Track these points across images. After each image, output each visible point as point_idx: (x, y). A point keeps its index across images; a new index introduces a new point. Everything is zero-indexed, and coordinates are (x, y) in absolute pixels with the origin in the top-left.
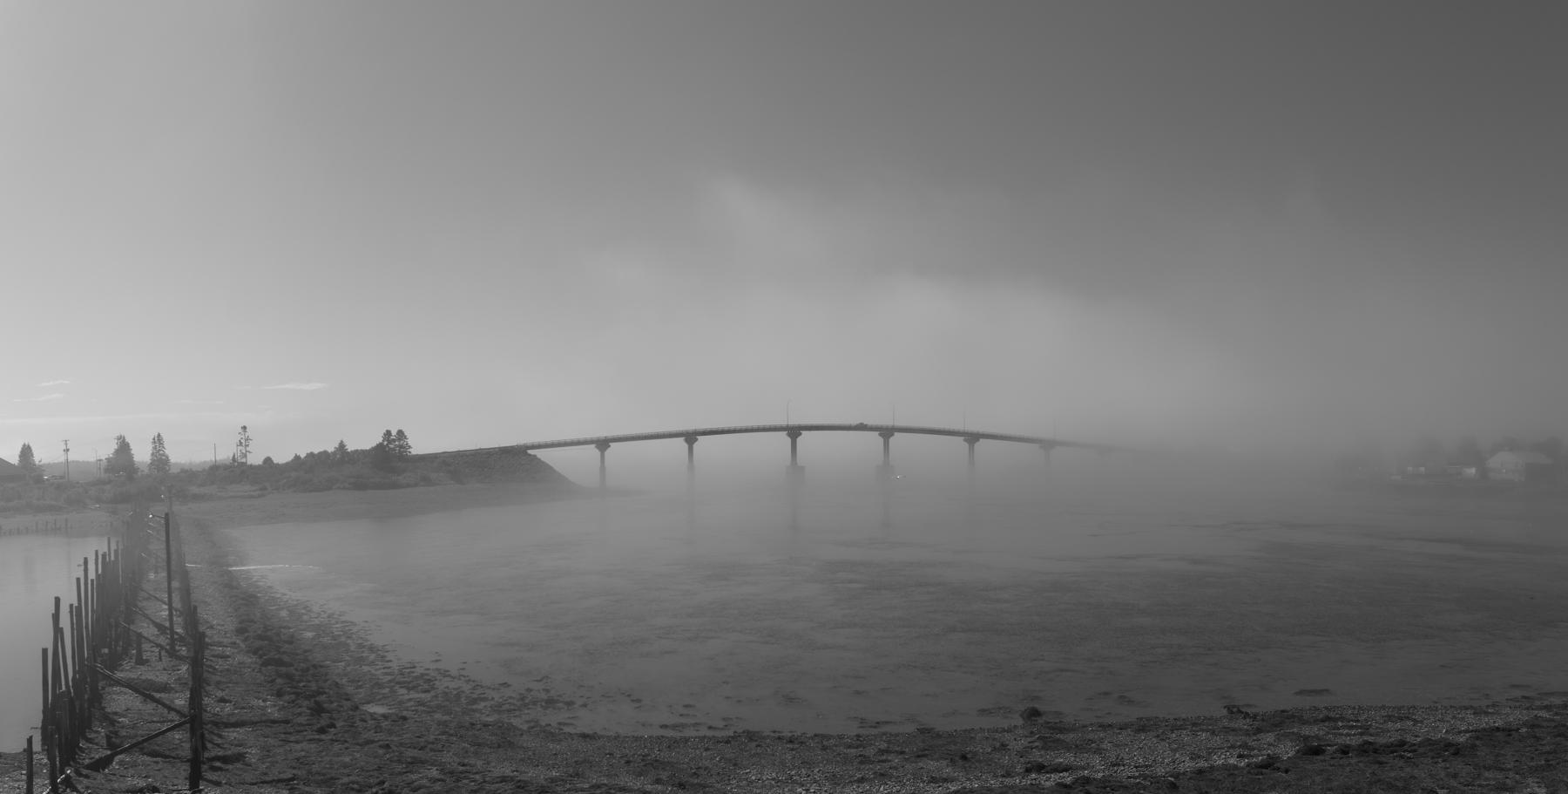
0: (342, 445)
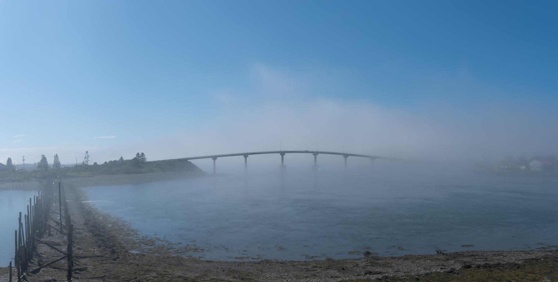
0: (122, 158)
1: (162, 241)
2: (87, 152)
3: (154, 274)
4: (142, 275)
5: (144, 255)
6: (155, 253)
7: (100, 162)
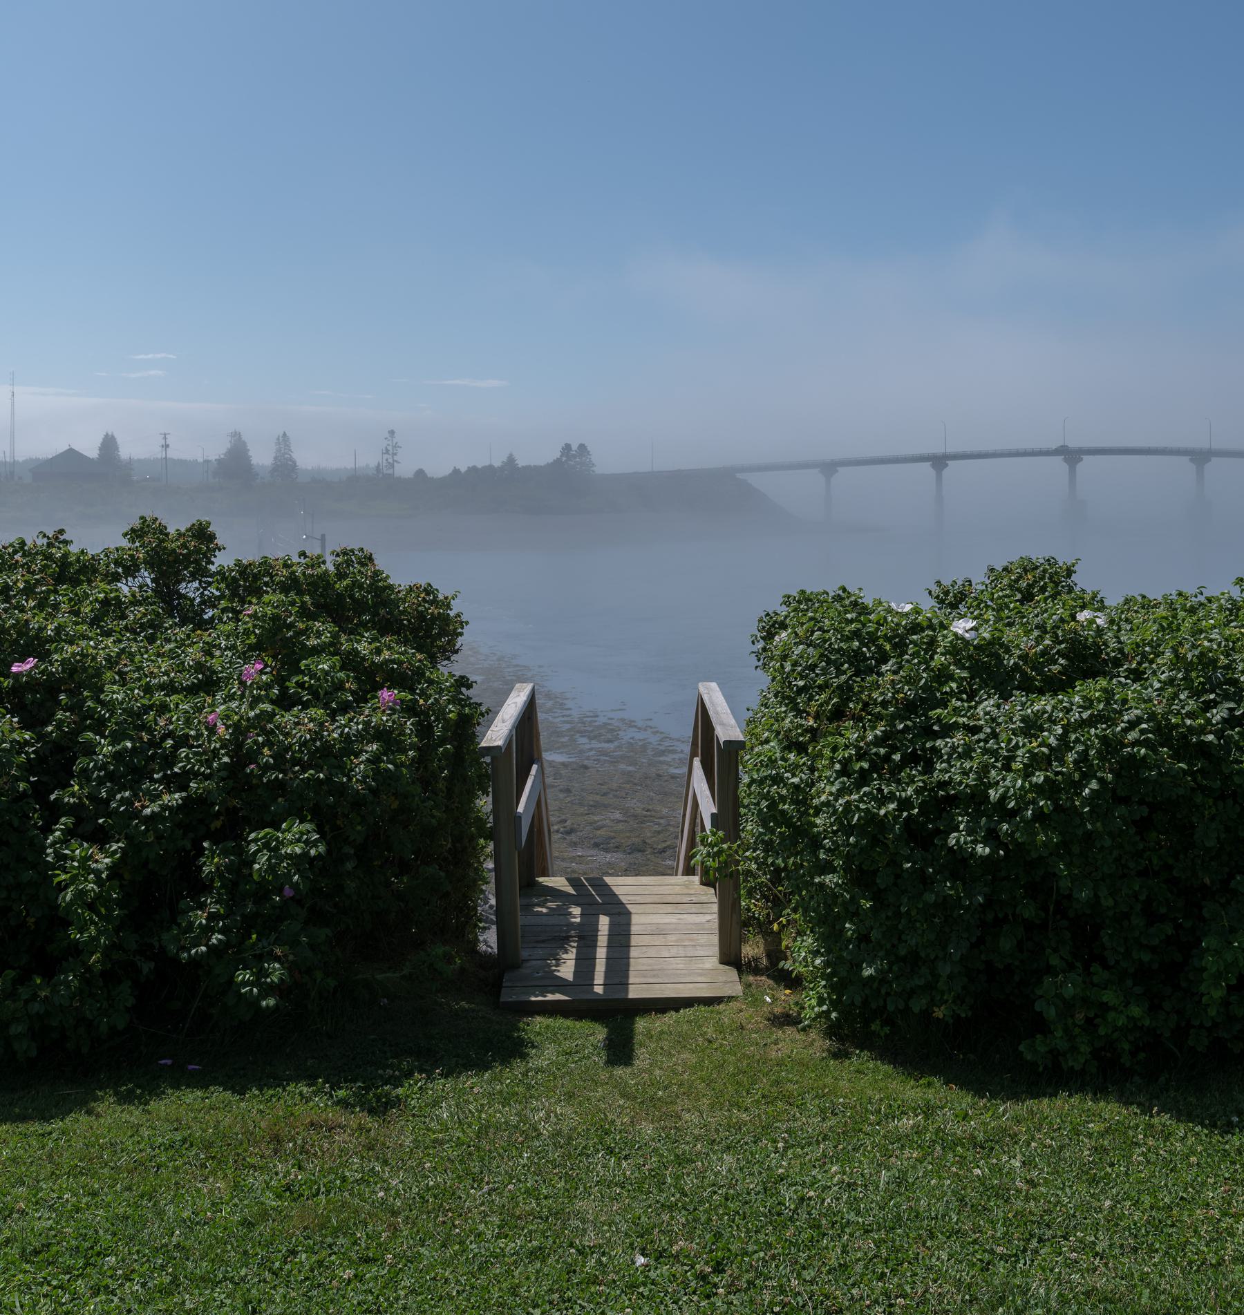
1: (639, 728)
2: (392, 433)
3: (617, 815)
4: (582, 815)
5: (586, 767)
6: (618, 762)
7: (438, 468)
